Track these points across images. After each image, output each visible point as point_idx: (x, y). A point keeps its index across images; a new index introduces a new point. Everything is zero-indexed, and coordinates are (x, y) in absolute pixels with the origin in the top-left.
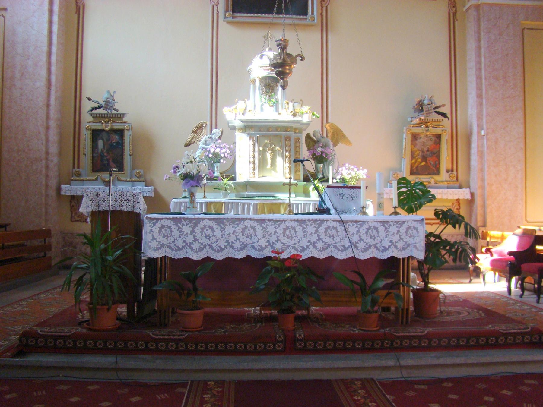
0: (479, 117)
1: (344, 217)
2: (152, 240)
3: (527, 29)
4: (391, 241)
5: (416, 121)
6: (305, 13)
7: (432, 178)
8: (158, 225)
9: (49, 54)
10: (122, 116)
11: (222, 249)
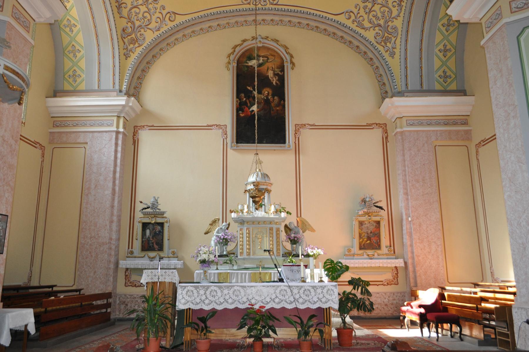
0: (407, 208)
1: (291, 284)
2: (182, 299)
3: (438, 146)
4: (318, 298)
5: (361, 213)
6: (284, 142)
7: (375, 252)
8: (186, 290)
9: (115, 172)
10: (163, 213)
11: (221, 303)
